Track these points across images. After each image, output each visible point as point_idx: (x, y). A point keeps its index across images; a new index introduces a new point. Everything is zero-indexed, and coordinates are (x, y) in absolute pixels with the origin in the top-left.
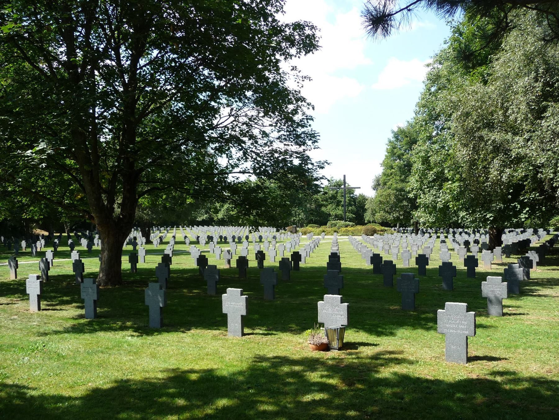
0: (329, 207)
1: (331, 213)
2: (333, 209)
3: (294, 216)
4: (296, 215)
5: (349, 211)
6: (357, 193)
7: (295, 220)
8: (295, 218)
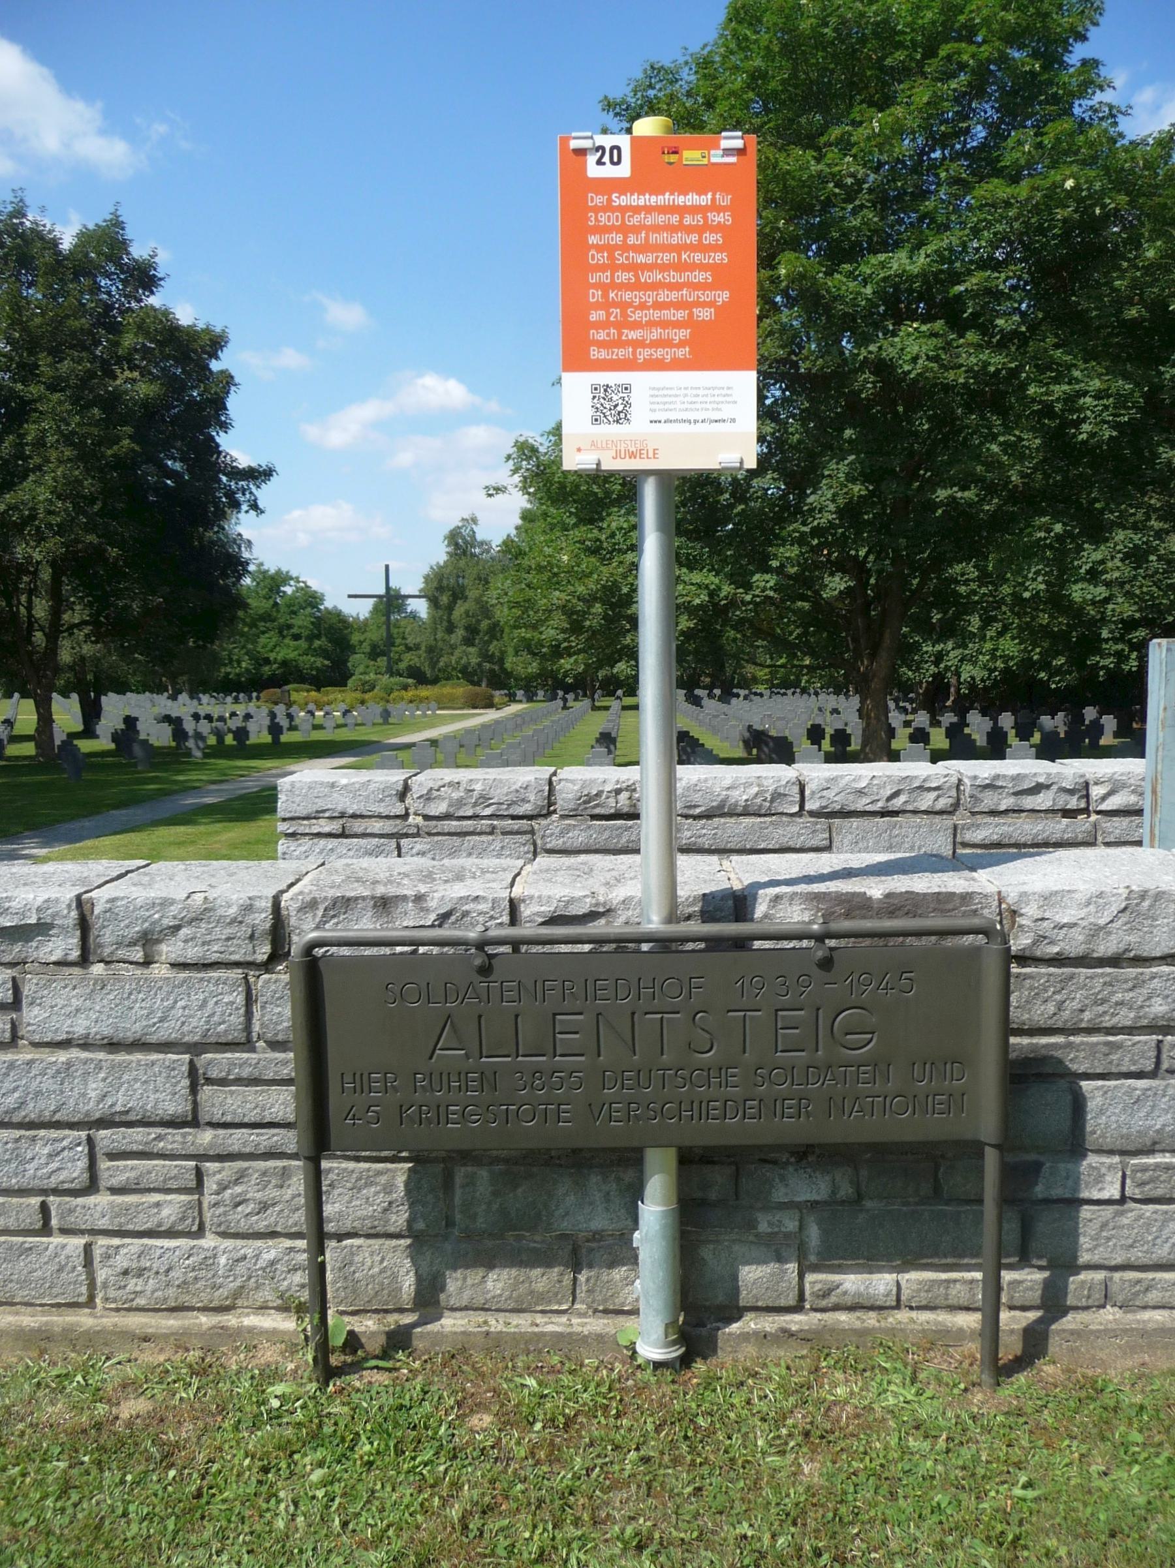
0: (263, 640)
1: (272, 656)
2: (275, 646)
3: (225, 665)
4: (231, 660)
5: (315, 650)
6: (328, 604)
7: (229, 673)
8: (229, 670)
